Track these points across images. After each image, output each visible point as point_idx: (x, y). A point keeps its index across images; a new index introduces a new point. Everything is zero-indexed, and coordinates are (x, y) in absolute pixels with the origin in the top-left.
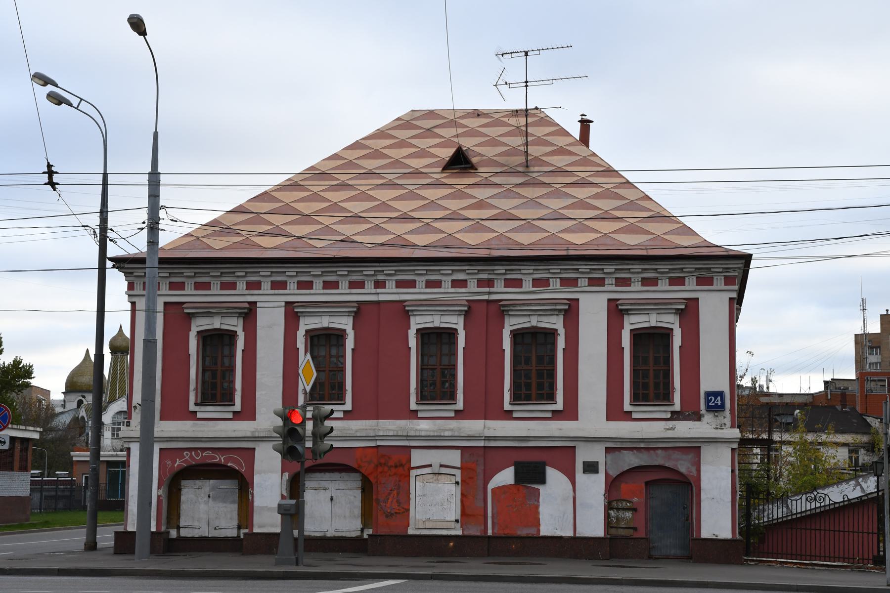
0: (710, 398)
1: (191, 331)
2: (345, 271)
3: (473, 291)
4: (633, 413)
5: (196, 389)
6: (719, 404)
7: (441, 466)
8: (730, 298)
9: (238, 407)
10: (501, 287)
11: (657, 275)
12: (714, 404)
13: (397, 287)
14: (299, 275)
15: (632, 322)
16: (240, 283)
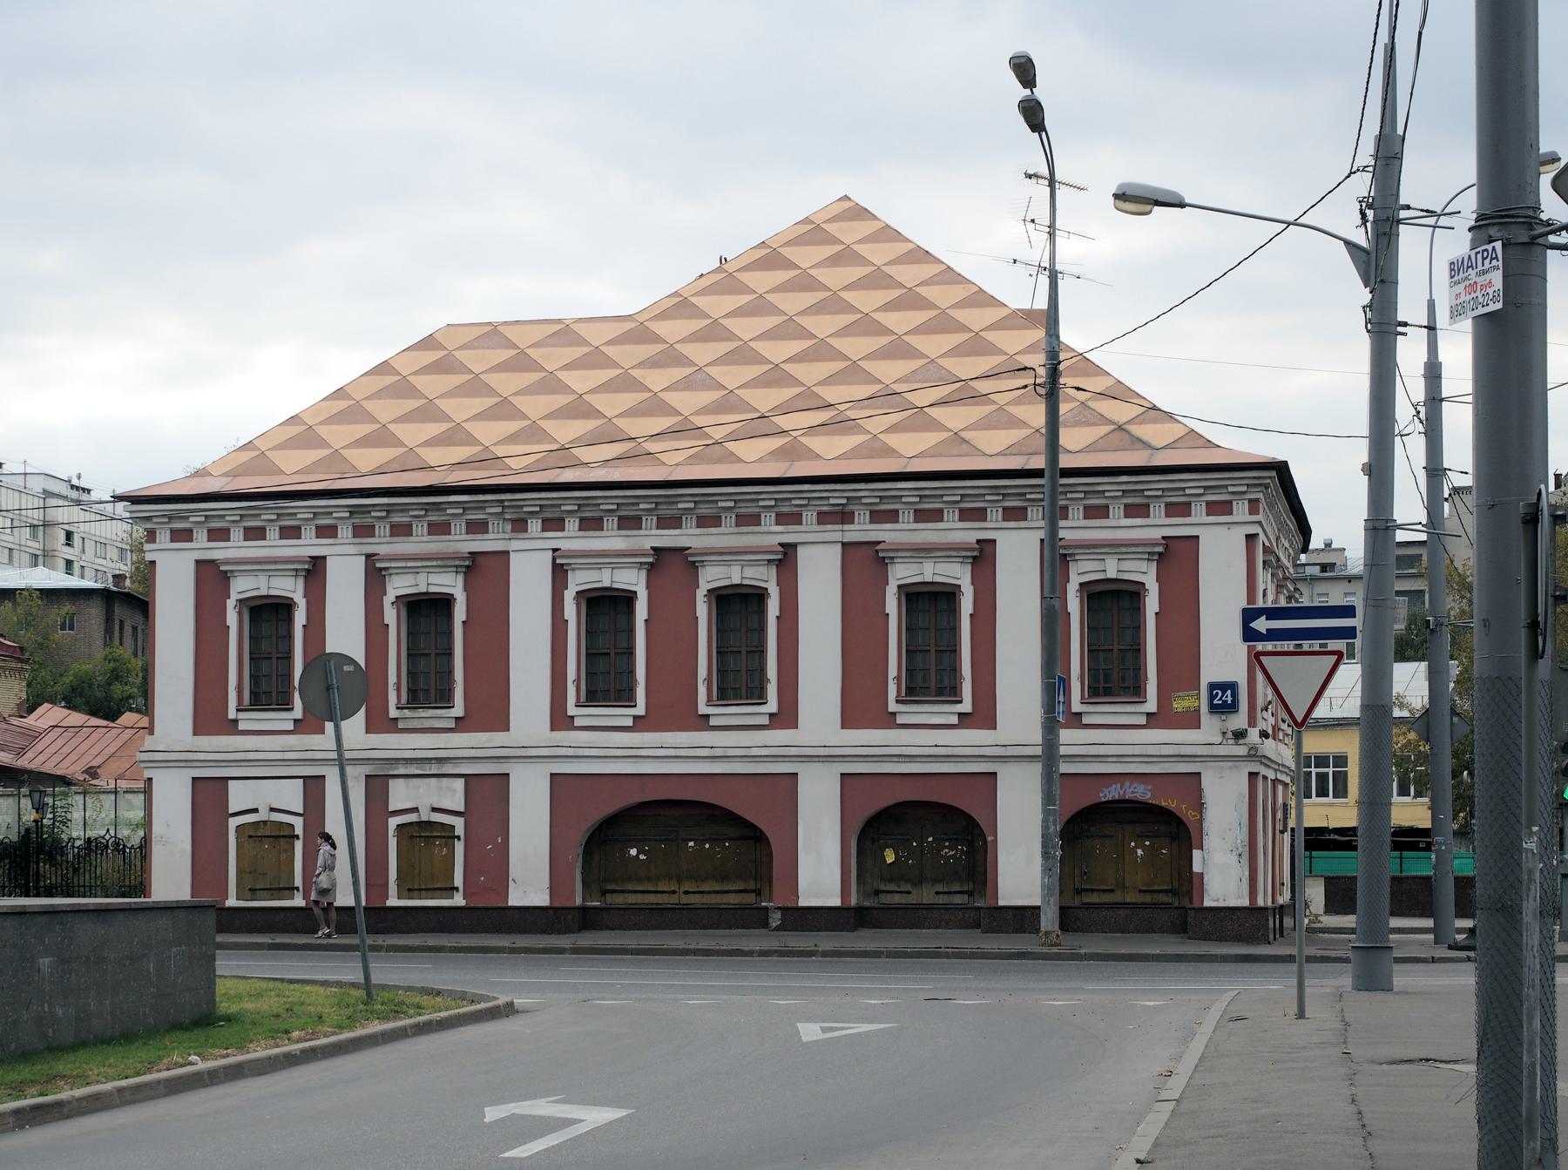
0: (1214, 693)
1: (567, 588)
2: (1242, 485)
3: (652, 537)
4: (897, 715)
5: (709, 680)
6: (1229, 702)
7: (272, 810)
8: (1247, 536)
9: (966, 706)
10: (1201, 515)
11: (484, 517)
12: (1220, 702)
13: (819, 523)
14: (1126, 495)
15: (399, 586)
16: (1073, 509)
